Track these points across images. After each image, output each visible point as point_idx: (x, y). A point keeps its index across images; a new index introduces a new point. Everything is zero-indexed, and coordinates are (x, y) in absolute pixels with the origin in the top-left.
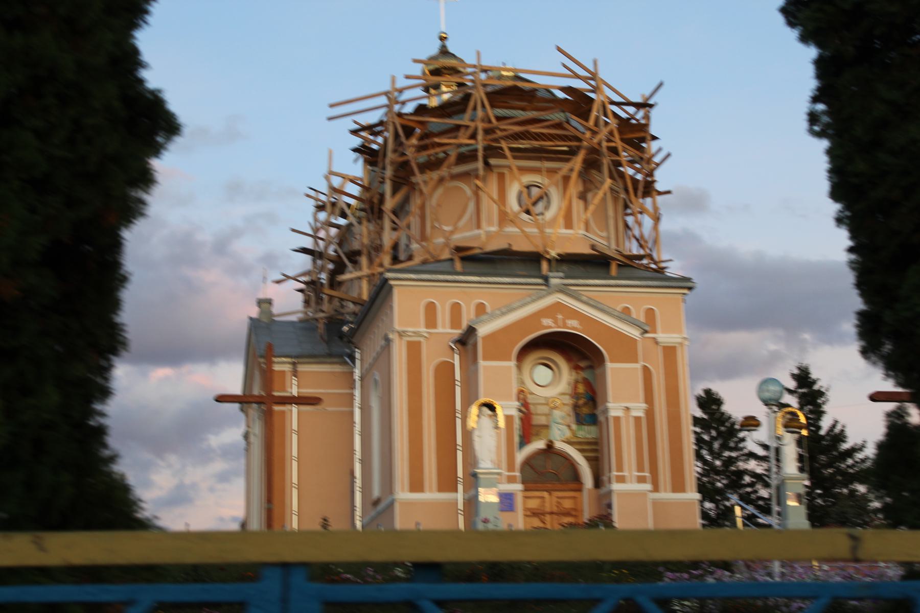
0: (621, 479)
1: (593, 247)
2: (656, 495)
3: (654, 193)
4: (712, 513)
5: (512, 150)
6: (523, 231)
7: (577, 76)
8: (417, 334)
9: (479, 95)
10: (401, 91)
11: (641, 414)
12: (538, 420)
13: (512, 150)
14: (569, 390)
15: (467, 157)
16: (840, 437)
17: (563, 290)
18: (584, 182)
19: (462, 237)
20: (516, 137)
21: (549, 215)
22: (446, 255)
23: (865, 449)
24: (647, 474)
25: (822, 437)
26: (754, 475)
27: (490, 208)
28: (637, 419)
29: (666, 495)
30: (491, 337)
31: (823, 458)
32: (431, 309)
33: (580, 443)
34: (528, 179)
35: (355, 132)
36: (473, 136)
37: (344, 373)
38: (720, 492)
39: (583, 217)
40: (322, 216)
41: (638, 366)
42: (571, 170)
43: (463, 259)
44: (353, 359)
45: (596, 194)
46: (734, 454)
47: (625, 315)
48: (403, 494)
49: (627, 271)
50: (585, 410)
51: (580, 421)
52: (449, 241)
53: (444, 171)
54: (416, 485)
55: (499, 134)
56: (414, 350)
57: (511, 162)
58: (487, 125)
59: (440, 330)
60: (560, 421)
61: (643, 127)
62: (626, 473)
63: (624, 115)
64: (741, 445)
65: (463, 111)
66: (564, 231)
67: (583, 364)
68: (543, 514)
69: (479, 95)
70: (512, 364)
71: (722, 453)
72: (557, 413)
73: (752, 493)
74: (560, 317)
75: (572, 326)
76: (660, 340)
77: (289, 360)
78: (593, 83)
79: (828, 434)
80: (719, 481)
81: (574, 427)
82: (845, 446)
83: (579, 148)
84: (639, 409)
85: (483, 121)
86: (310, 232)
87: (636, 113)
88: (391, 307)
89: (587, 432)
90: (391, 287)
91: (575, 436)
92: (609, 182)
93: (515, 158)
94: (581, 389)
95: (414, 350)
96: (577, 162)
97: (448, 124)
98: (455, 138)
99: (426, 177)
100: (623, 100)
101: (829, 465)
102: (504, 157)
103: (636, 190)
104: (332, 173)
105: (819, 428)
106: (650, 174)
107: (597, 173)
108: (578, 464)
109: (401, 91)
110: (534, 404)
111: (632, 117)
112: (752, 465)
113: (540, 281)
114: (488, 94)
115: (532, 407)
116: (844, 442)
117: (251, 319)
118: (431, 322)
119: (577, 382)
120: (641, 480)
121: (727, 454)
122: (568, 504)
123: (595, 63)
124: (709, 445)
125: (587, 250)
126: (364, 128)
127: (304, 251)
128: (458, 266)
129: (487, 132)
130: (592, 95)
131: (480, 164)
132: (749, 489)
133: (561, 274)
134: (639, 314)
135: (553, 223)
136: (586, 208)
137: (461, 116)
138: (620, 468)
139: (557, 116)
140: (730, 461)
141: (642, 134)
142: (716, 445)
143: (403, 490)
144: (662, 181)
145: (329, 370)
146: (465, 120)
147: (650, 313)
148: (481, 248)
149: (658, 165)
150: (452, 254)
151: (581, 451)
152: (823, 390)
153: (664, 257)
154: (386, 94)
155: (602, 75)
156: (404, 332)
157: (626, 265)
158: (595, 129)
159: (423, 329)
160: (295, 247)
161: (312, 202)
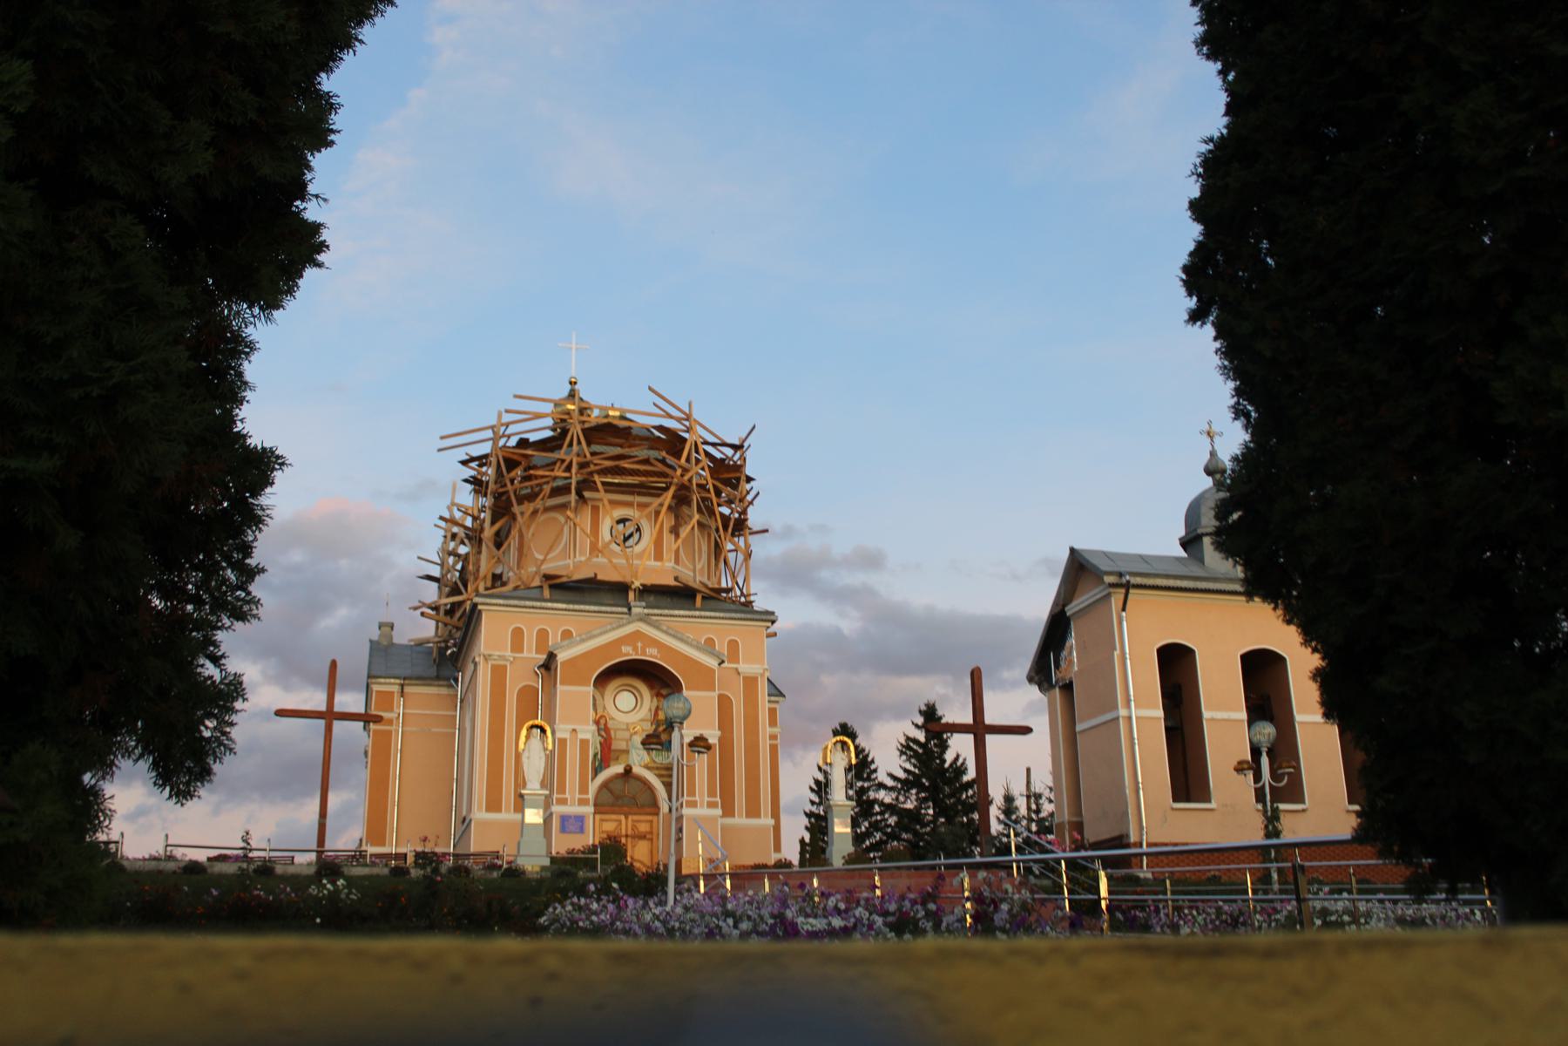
0: (693, 804)
1: (676, 579)
2: (728, 821)
3: (748, 531)
5: (604, 484)
6: (611, 562)
7: (670, 416)
8: (502, 657)
9: (576, 430)
10: (507, 425)
12: (617, 745)
13: (604, 484)
14: (650, 717)
15: (564, 490)
17: (643, 619)
18: (677, 517)
19: (550, 567)
20: (605, 472)
21: (638, 549)
22: (537, 582)
24: (718, 799)
25: (947, 770)
26: (882, 804)
29: (740, 820)
30: (571, 662)
32: (518, 634)
33: (657, 768)
34: (620, 513)
35: (464, 463)
36: (568, 469)
37: (449, 695)
39: (674, 547)
40: (452, 545)
42: (661, 505)
43: (552, 587)
44: (456, 680)
45: (685, 528)
46: (866, 785)
48: (480, 814)
49: (712, 603)
53: (538, 504)
55: (592, 467)
56: (499, 673)
57: (602, 494)
58: (581, 460)
59: (525, 654)
61: (738, 468)
62: (567, 795)
63: (719, 455)
64: (874, 776)
65: (560, 447)
66: (653, 563)
69: (576, 430)
70: (591, 688)
73: (881, 821)
74: (639, 645)
75: (652, 655)
77: (398, 681)
78: (687, 423)
79: (951, 765)
83: (671, 483)
85: (578, 455)
86: (439, 562)
87: (734, 455)
88: (481, 631)
90: (480, 611)
92: (697, 517)
93: (606, 491)
95: (499, 673)
96: (668, 498)
97: (551, 458)
98: (553, 470)
99: (523, 508)
100: (718, 441)
102: (597, 490)
103: (725, 528)
104: (453, 504)
106: (744, 512)
107: (687, 507)
109: (507, 425)
110: (616, 730)
111: (731, 459)
112: (882, 795)
113: (625, 610)
114: (583, 430)
115: (612, 733)
117: (371, 641)
118: (517, 645)
120: (711, 805)
121: (859, 784)
122: (643, 828)
123: (690, 405)
125: (673, 583)
126: (473, 459)
127: (429, 578)
128: (547, 593)
129: (582, 466)
130: (686, 435)
131: (573, 497)
132: (879, 818)
133: (644, 604)
134: (722, 647)
135: (640, 556)
136: (676, 541)
137: (557, 452)
138: (692, 793)
139: (643, 453)
141: (738, 475)
144: (755, 518)
145: (437, 692)
146: (561, 454)
147: (733, 645)
148: (567, 576)
149: (751, 503)
150: (541, 582)
151: (659, 776)
153: (752, 591)
154: (492, 427)
155: (695, 415)
156: (490, 655)
157: (711, 598)
159: (508, 653)
160: (422, 574)
161: (442, 533)
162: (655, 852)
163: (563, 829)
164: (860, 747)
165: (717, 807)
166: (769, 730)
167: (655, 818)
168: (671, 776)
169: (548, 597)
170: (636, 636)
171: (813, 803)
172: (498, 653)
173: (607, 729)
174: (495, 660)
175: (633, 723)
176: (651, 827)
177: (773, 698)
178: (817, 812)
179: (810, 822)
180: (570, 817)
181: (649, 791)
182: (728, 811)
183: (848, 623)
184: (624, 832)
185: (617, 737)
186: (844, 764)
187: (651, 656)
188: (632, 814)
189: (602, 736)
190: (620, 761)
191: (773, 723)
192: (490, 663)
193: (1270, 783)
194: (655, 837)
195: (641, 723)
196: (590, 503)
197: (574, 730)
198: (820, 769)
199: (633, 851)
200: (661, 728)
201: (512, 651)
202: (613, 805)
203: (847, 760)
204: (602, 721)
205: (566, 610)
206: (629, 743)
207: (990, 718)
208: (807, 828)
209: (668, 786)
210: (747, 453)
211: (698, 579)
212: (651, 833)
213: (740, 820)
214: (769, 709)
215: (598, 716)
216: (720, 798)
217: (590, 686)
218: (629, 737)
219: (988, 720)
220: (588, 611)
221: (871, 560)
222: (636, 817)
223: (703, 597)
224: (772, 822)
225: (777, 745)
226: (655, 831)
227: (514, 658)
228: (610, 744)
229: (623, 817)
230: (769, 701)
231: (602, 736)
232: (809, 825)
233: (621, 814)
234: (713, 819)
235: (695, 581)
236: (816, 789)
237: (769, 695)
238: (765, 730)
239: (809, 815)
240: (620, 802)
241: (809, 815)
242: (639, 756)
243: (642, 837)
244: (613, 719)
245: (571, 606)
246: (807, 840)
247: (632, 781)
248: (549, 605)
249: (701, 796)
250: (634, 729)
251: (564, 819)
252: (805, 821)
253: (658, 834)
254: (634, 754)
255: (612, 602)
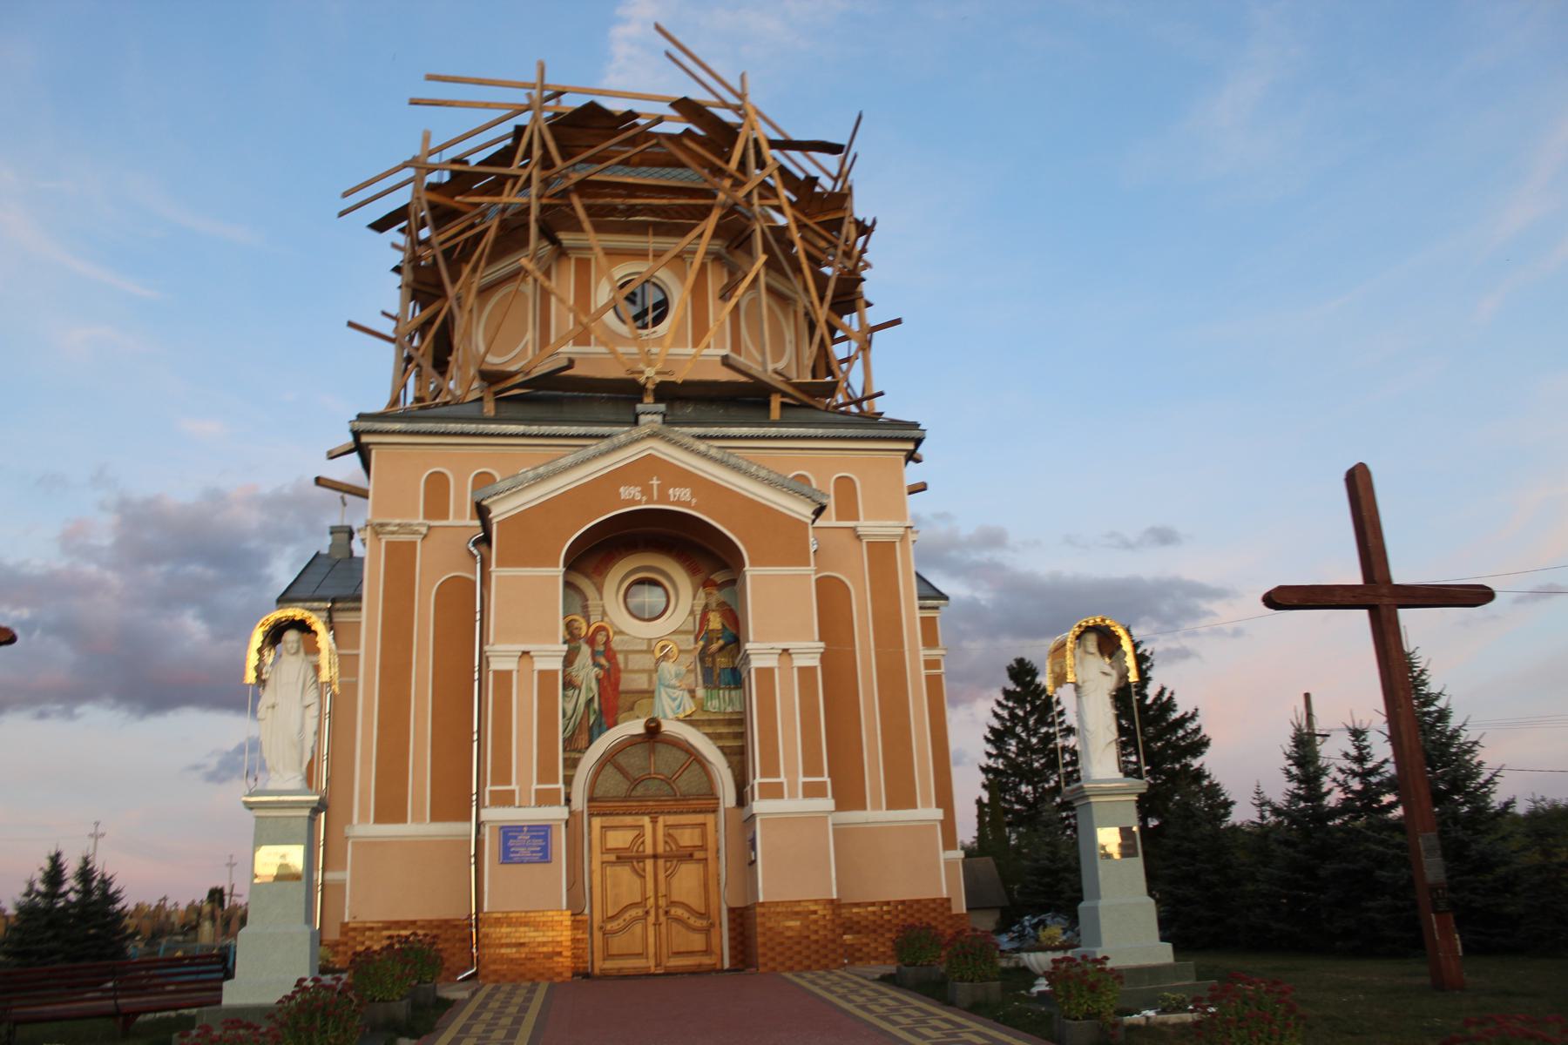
2: (853, 817)
4: (1030, 797)
6: (613, 352)
11: (815, 662)
12: (632, 681)
16: (1169, 706)
18: (731, 274)
23: (1197, 718)
24: (826, 779)
27: (562, 318)
28: (806, 672)
29: (876, 815)
31: (1151, 730)
32: (437, 487)
33: (710, 722)
38: (1036, 772)
41: (810, 572)
47: (799, 487)
49: (803, 414)
50: (722, 661)
51: (711, 678)
52: (1262, 796)
54: (390, 808)
59: (451, 521)
60: (674, 682)
61: (841, 199)
67: (719, 577)
68: (641, 858)
71: (1039, 729)
72: (668, 668)
75: (680, 500)
76: (861, 531)
79: (1155, 701)
80: (1037, 761)
81: (700, 692)
82: (1175, 716)
84: (809, 653)
89: (721, 703)
91: (701, 707)
93: (599, 228)
94: (715, 622)
101: (1158, 737)
105: (1146, 697)
108: (710, 763)
110: (627, 653)
115: (620, 658)
116: (1174, 711)
119: (706, 610)
120: (812, 791)
121: (1043, 730)
122: (688, 838)
123: (743, 78)
124: (1024, 721)
128: (489, 408)
140: (1049, 738)
142: (1031, 722)
143: (364, 818)
147: (845, 486)
151: (713, 737)
152: (1147, 654)
156: (382, 525)
157: (804, 406)
158: (738, 175)
162: (712, 884)
163: (507, 856)
164: (1042, 687)
165: (823, 794)
166: (923, 653)
167: (710, 818)
169: (492, 413)
171: (989, 755)
172: (398, 521)
173: (609, 654)
174: (393, 533)
175: (661, 639)
176: (704, 836)
177: (929, 603)
178: (995, 766)
179: (988, 779)
180: (519, 829)
181: (695, 766)
182: (849, 794)
183: (984, 595)
184: (649, 850)
185: (630, 667)
186: (1110, 683)
187: (678, 503)
188: (662, 813)
190: (636, 712)
191: (930, 639)
192: (385, 539)
194: (711, 855)
195: (674, 637)
196: (573, 256)
197: (525, 653)
199: (668, 885)
200: (715, 647)
201: (426, 516)
202: (627, 798)
203: (1114, 674)
204: (601, 638)
205: (523, 435)
206: (655, 676)
207: (1403, 572)
208: (984, 786)
210: (851, 177)
211: (770, 367)
212: (703, 848)
213: (876, 815)
214: (922, 619)
215: (592, 629)
216: (830, 776)
217: (557, 566)
218: (652, 666)
219: (1403, 572)
220: (567, 436)
221: (994, 539)
222: (671, 819)
223: (784, 405)
224: (939, 814)
225: (939, 677)
226: (711, 844)
227: (430, 528)
228: (617, 682)
229: (646, 820)
230: (921, 608)
232: (987, 783)
233: (643, 814)
234: (818, 819)
235: (765, 371)
236: (992, 738)
237: (920, 598)
238: (915, 655)
239: (986, 770)
240: (640, 791)
241: (986, 770)
242: (674, 700)
243: (687, 856)
244: (621, 633)
245: (534, 429)
246: (986, 799)
247: (661, 748)
248: (493, 428)
249: (791, 772)
250: (663, 647)
251: (508, 833)
252: (982, 778)
253: (718, 851)
254: (664, 696)
255: (612, 418)
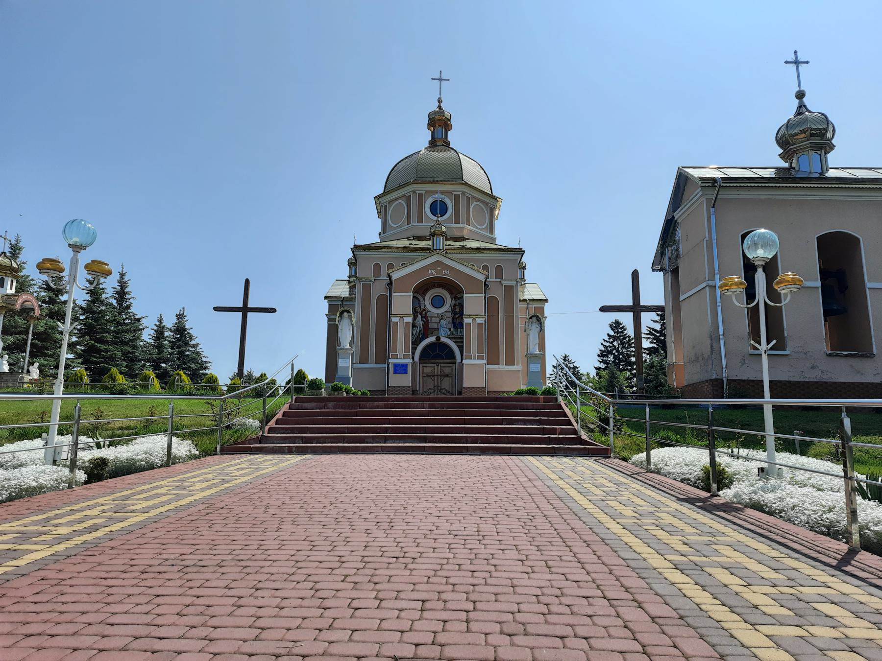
32: (377, 266)
75: (446, 274)
122: (447, 370)
168: (463, 342)
170: (438, 263)
187: (446, 275)
189: (424, 321)
193: (766, 303)
198: (602, 344)
204: (424, 313)
209: (461, 348)
222: (443, 365)
231: (424, 321)
244: (430, 311)
251: (396, 365)
